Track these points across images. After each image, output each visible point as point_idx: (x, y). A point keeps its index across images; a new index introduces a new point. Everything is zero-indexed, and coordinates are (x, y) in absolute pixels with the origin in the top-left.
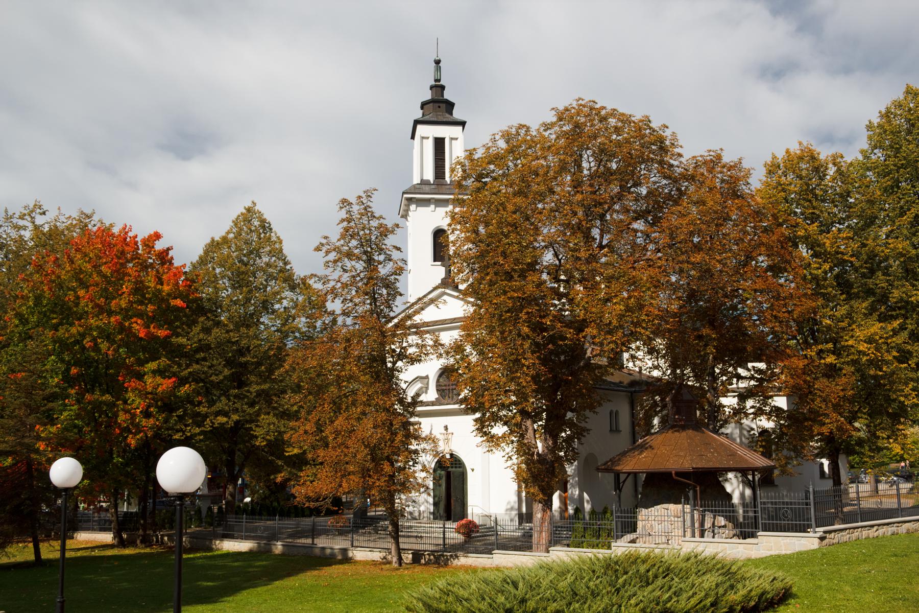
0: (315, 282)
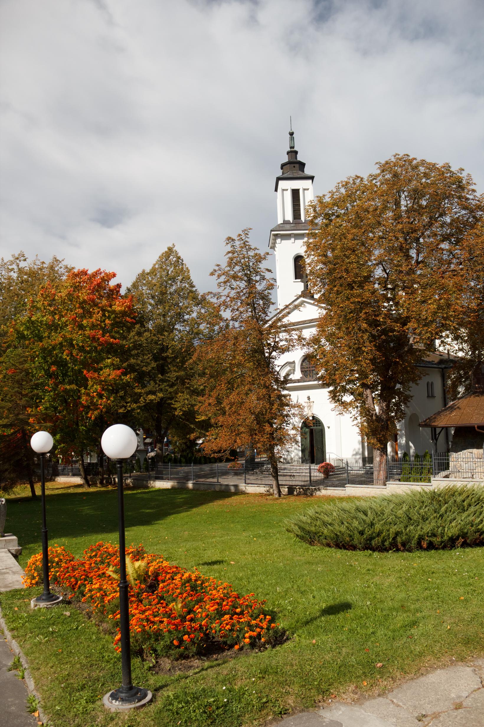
0: (211, 297)
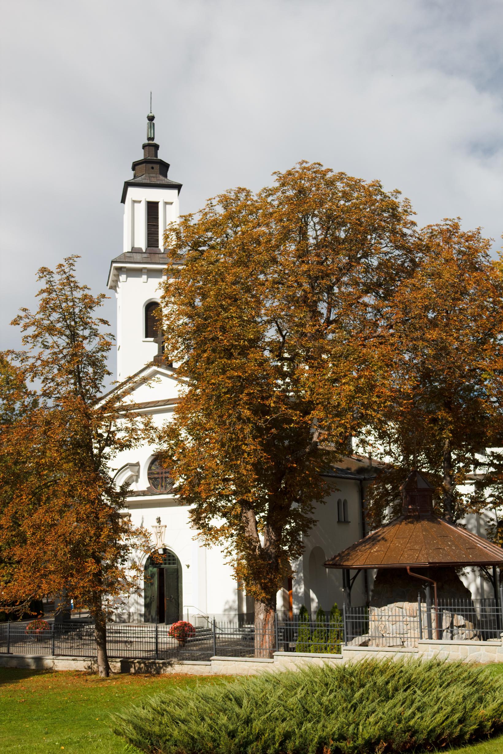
0: (12, 359)
